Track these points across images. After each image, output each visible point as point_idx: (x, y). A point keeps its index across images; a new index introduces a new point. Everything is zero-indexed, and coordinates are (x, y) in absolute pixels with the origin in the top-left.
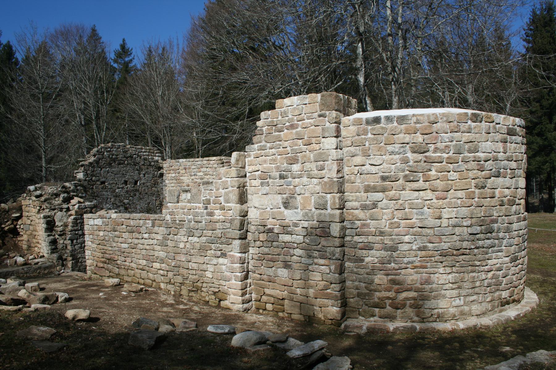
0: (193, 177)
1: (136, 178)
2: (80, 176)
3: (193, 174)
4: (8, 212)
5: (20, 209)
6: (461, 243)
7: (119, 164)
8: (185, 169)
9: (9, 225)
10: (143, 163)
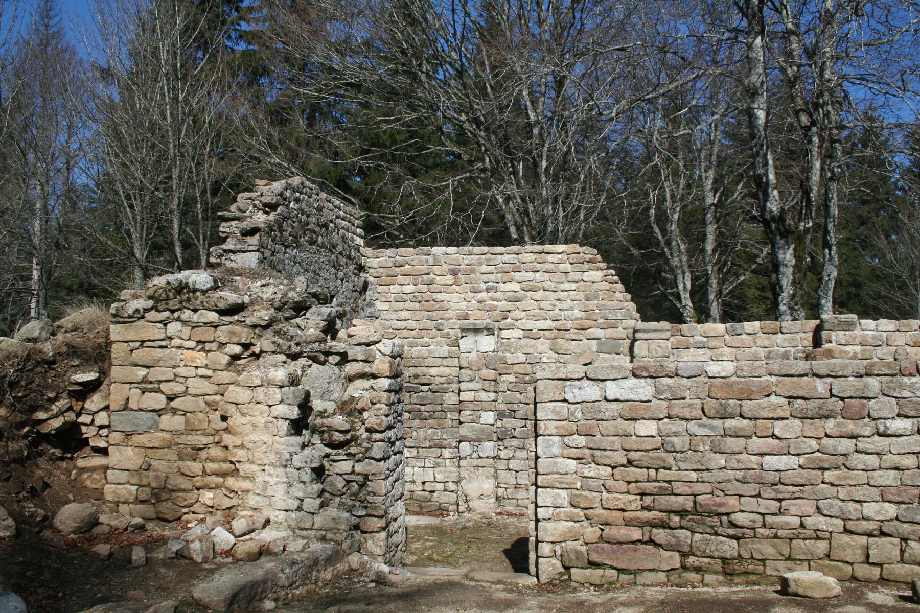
0: (483, 295)
3: (483, 286)
4: (51, 363)
5: (99, 355)
8: (454, 273)
9: (62, 413)
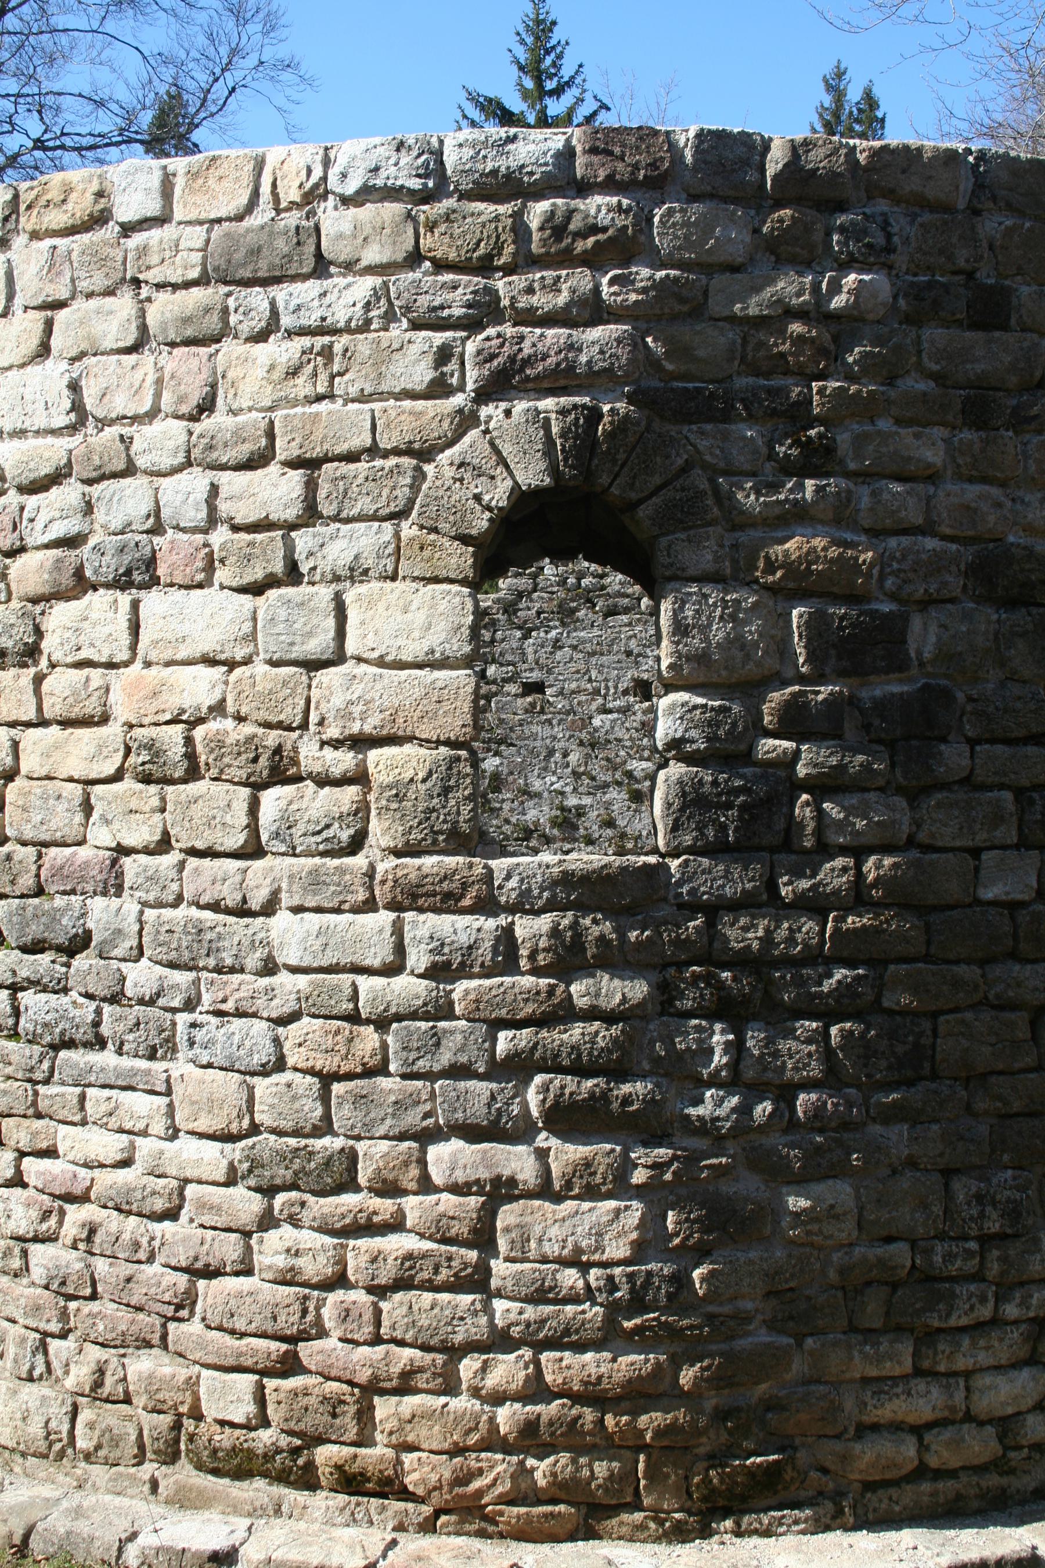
7: (611, 612)
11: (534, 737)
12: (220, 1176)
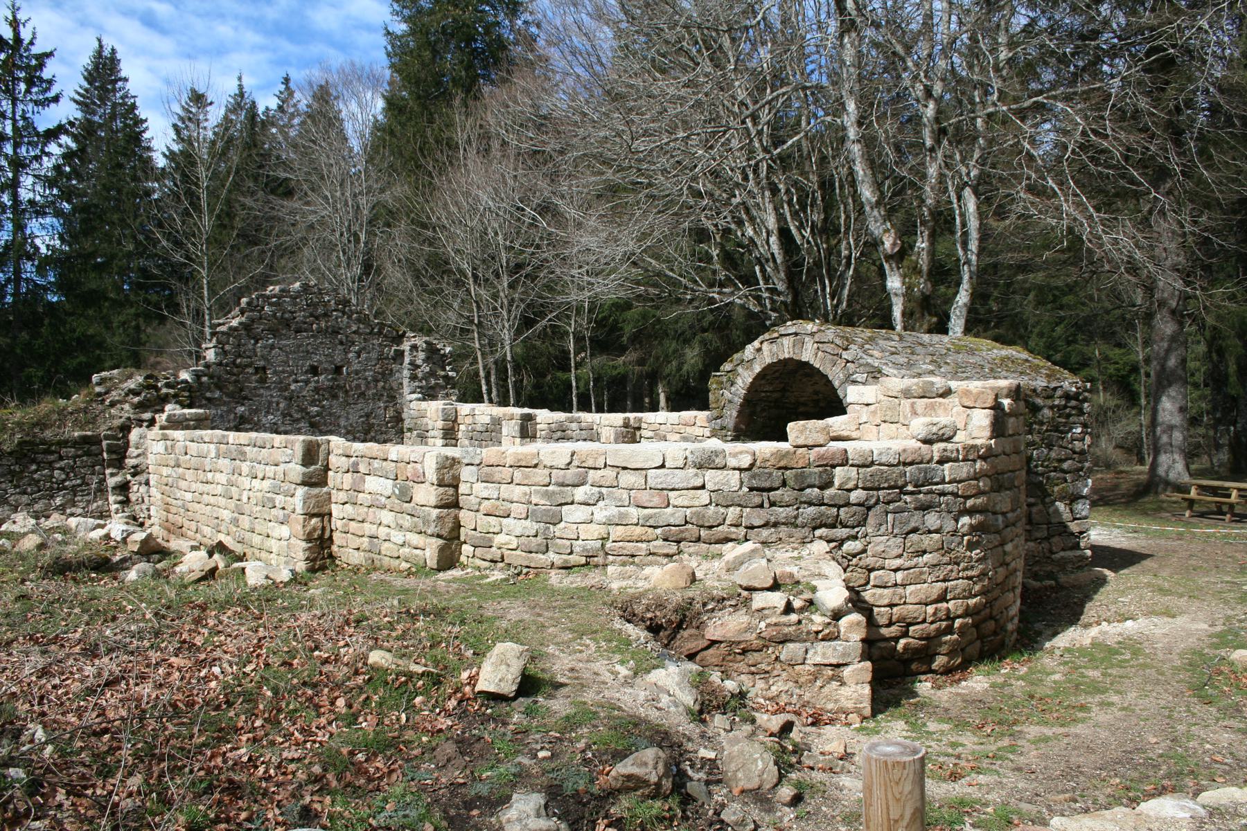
1: (338, 359)
2: (210, 355)
6: (722, 510)
7: (298, 331)
10: (354, 328)
11: (261, 395)
12: (524, 516)
